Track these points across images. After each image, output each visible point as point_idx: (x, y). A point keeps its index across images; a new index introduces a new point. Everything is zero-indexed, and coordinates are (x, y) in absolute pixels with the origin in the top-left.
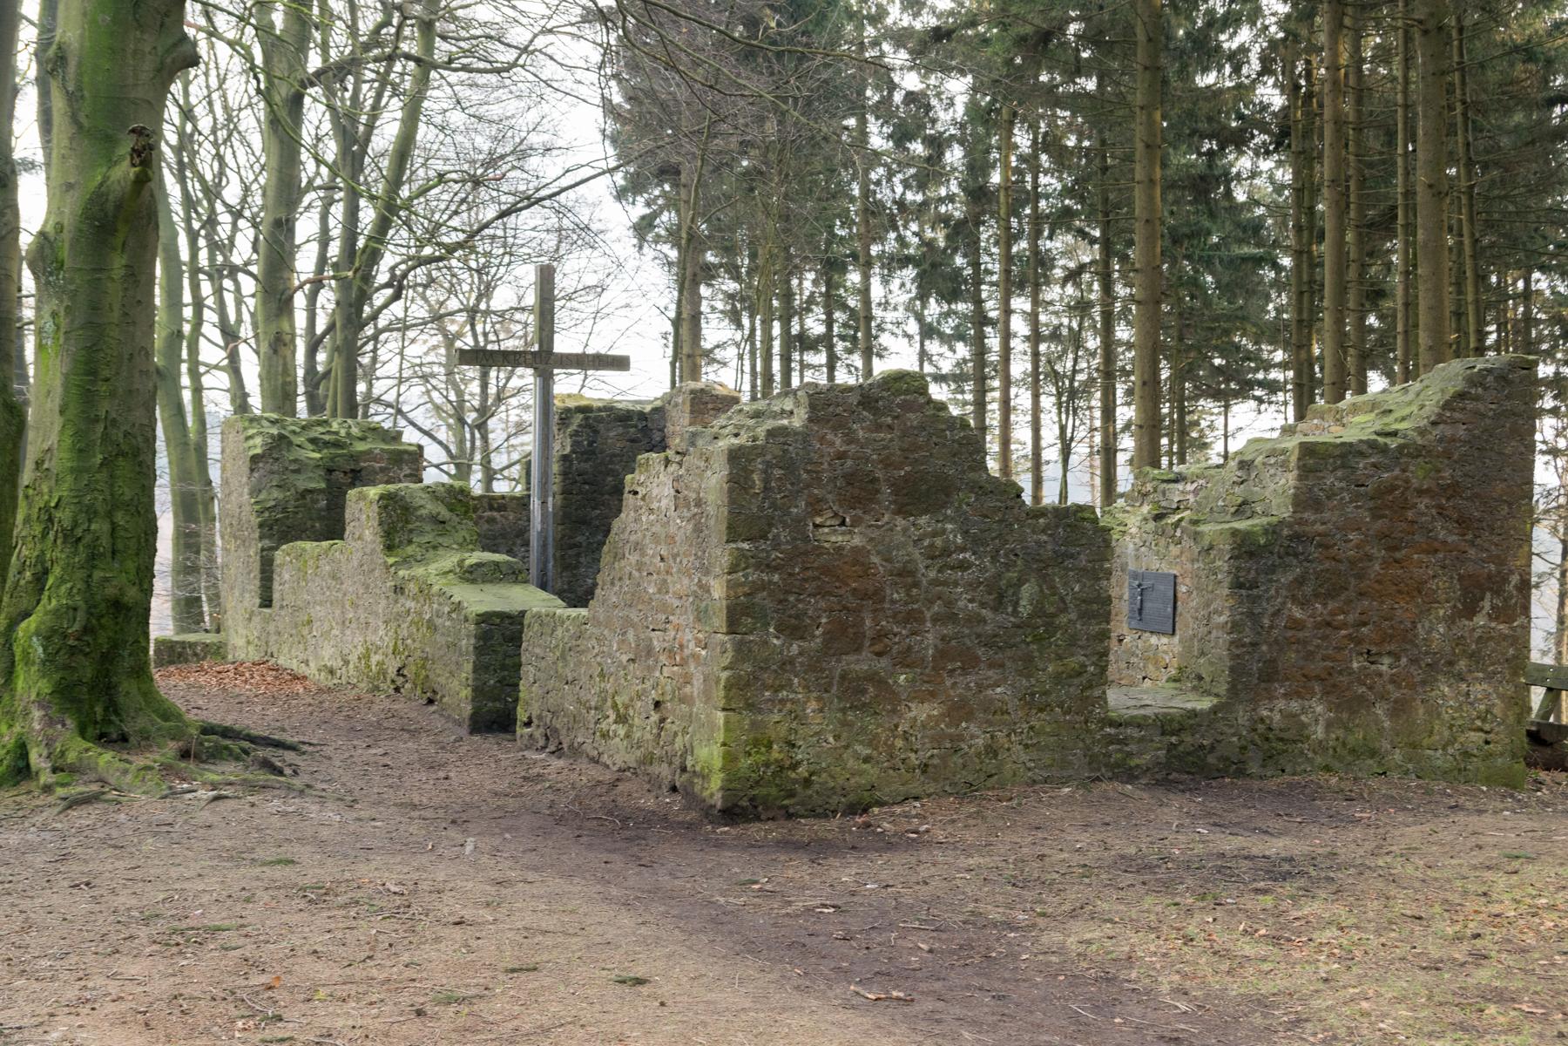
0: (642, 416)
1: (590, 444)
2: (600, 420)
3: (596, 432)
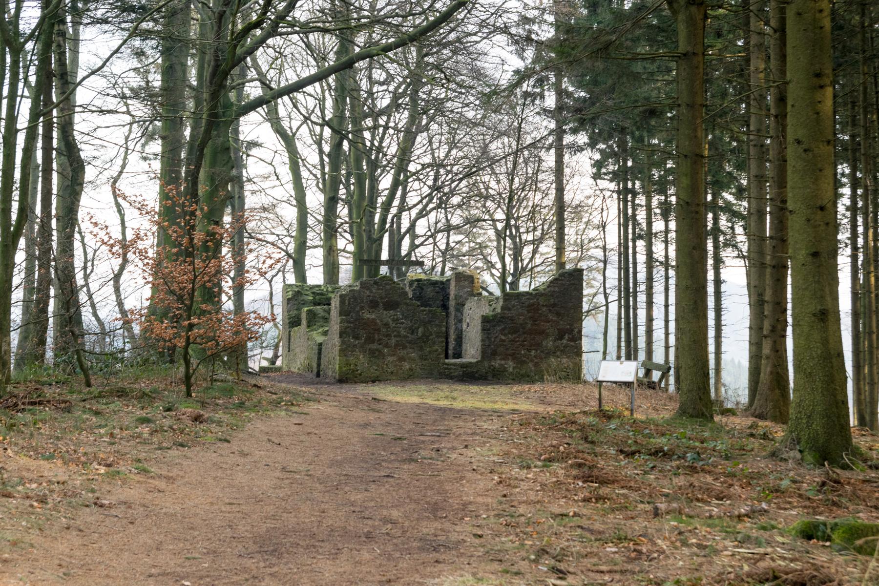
0: (442, 283)
2: (424, 285)
3: (422, 289)
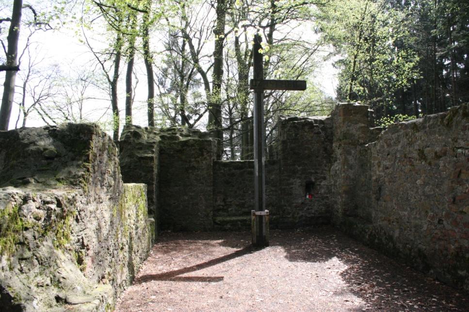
1: (296, 135)
